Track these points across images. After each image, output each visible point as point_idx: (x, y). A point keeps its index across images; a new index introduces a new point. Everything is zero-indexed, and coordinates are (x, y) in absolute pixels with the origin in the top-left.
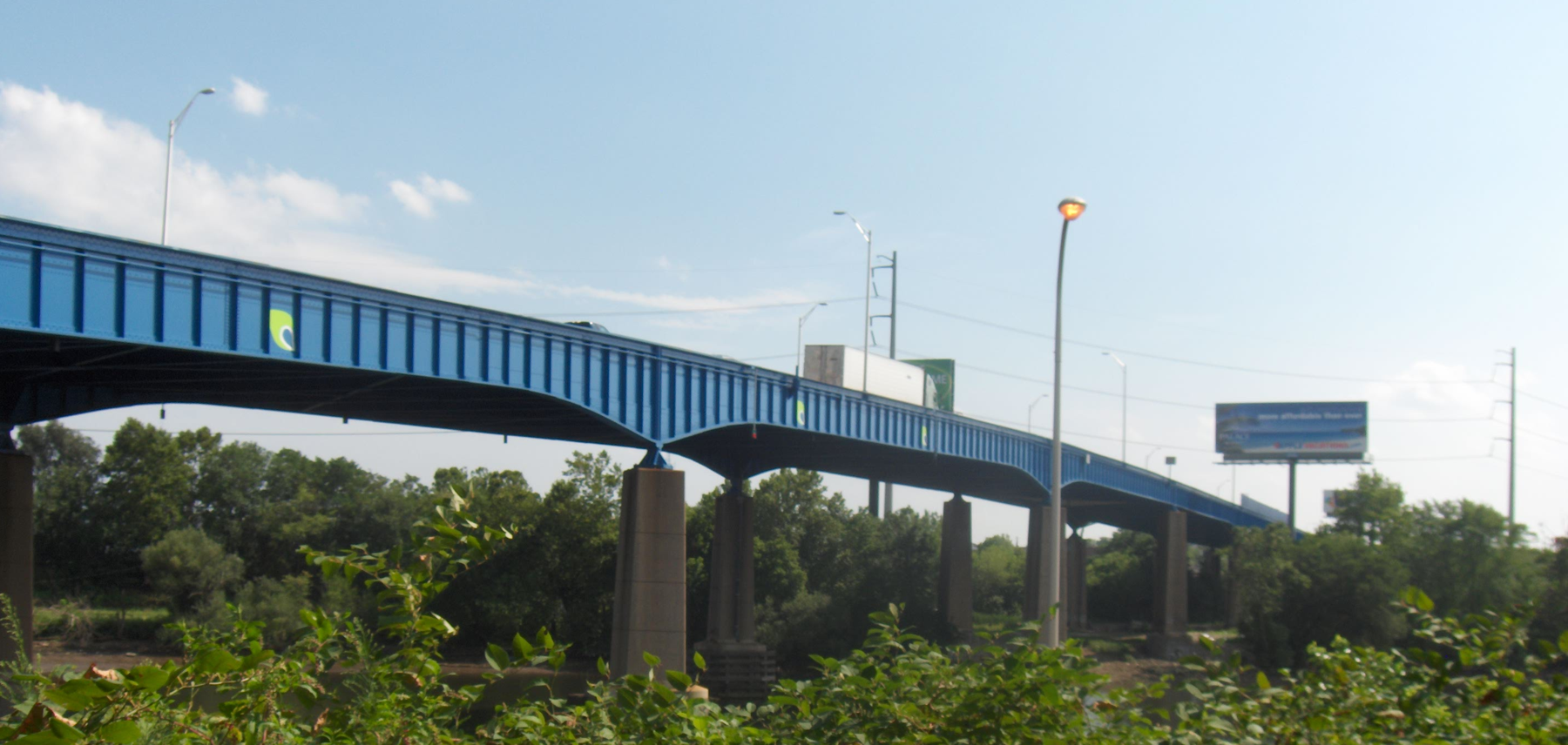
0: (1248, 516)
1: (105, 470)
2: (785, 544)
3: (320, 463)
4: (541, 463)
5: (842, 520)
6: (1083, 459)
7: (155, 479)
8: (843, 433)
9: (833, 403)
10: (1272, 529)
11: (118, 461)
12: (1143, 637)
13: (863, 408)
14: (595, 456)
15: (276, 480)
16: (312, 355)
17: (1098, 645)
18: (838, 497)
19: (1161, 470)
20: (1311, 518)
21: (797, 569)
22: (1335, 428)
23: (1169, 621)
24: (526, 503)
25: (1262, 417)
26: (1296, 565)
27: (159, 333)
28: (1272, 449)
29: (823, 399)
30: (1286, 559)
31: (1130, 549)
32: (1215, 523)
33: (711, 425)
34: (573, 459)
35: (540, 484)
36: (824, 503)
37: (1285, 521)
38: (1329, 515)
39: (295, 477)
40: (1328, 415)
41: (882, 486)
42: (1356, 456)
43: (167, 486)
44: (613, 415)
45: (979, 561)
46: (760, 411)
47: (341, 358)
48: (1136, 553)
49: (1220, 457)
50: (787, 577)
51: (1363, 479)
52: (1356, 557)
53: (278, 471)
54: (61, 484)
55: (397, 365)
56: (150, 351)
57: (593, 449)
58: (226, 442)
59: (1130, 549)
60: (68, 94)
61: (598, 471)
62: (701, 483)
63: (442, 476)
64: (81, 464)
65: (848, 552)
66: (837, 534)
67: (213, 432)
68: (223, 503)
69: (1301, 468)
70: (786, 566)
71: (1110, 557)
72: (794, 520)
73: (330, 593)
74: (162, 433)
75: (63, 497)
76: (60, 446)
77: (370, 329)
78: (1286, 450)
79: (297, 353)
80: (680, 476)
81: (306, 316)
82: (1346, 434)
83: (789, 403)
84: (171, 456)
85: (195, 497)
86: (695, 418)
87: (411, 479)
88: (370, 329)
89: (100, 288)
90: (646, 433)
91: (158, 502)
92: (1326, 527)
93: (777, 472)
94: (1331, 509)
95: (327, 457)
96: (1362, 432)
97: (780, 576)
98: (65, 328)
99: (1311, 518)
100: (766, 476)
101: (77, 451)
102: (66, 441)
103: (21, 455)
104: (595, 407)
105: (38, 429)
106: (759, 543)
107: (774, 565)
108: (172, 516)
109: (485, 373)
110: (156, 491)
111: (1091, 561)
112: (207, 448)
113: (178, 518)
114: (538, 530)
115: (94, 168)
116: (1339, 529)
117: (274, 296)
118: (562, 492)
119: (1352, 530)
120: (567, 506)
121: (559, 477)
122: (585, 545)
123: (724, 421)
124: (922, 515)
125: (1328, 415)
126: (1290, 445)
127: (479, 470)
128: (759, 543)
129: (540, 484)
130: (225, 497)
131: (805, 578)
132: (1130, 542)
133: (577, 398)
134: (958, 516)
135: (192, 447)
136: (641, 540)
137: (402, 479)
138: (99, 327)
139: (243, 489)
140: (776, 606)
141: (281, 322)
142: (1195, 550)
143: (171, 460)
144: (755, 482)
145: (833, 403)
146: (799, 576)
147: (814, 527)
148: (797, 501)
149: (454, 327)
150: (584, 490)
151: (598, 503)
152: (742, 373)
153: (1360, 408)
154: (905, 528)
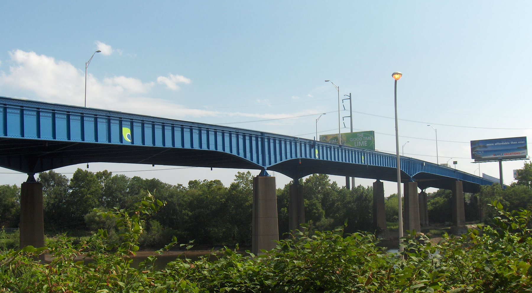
0: (485, 181)
1: (71, 187)
2: (316, 201)
3: (147, 180)
4: (226, 177)
5: (337, 191)
6: (423, 164)
7: (88, 190)
8: (333, 160)
9: (328, 149)
10: (494, 185)
11: (75, 184)
12: (450, 228)
13: (340, 150)
14: (245, 173)
15: (132, 188)
16: (138, 143)
17: (433, 231)
18: (334, 183)
19: (453, 166)
20: (509, 180)
21: (321, 210)
22: (515, 147)
23: (459, 221)
24: (222, 191)
25: (488, 145)
26: (504, 198)
27: (83, 138)
28: (492, 156)
29: (325, 148)
30: (500, 196)
31: (443, 196)
32: (472, 184)
33: (284, 160)
34: (238, 175)
35: (227, 184)
36: (329, 185)
37: (499, 181)
38: (516, 179)
39: (139, 186)
40: (512, 143)
41: (351, 178)
42: (524, 157)
43: (93, 192)
44: (248, 158)
45: (388, 204)
46: (302, 154)
47: (149, 143)
48: (446, 197)
49: (473, 160)
50: (317, 213)
51: (526, 165)
52: (526, 194)
53: (132, 185)
54: (55, 193)
55: (169, 145)
56: (80, 143)
57: (245, 171)
58: (113, 175)
59: (443, 196)
60: (127, 76)
61: (247, 179)
62: (282, 181)
63: (190, 183)
64: (62, 185)
65: (339, 203)
66: (335, 196)
67: (109, 172)
68: (114, 197)
69: (503, 163)
70: (317, 209)
71: (436, 199)
72: (319, 192)
73: (153, 227)
74: (90, 173)
75: (56, 198)
76: (54, 180)
77: (178, 134)
78: (498, 156)
79: (133, 142)
80: (274, 178)
81: (135, 129)
82: (519, 149)
83: (312, 150)
84: (94, 181)
85: (103, 195)
86: (294, 155)
87: (180, 185)
88: (178, 134)
89: (61, 123)
90: (261, 164)
91: (90, 198)
92: (514, 183)
93: (312, 175)
94: (516, 176)
95: (150, 178)
96: (525, 148)
97: (315, 213)
98: (50, 138)
99: (509, 180)
100: (308, 177)
101: (60, 181)
102: (56, 178)
103: (38, 183)
104: (242, 155)
105: (46, 174)
106: (306, 201)
107: (313, 209)
108: (95, 203)
109: (201, 146)
110: (89, 194)
111: (429, 201)
112: (106, 178)
113: (97, 203)
114: (227, 201)
115: (46, 79)
116: (519, 184)
117: (123, 123)
118: (234, 187)
119: (524, 184)
120: (236, 191)
121: (233, 181)
122: (244, 205)
123: (289, 158)
124: (367, 188)
125: (512, 143)
126: (499, 154)
127: (204, 181)
128: (306, 201)
129: (227, 184)
130: (114, 195)
131: (324, 213)
132: (443, 193)
133: (234, 153)
134: (379, 188)
135: (101, 178)
136: (261, 203)
137: (177, 185)
138: (61, 137)
139: (120, 192)
140: (314, 224)
141: (126, 132)
142: (468, 195)
143: (94, 183)
144: (304, 179)
145: (328, 149)
146: (322, 213)
147: (326, 195)
148: (320, 185)
149: (206, 132)
150: (242, 185)
151: (247, 190)
152: (294, 140)
153: (524, 139)
154: (359, 194)
